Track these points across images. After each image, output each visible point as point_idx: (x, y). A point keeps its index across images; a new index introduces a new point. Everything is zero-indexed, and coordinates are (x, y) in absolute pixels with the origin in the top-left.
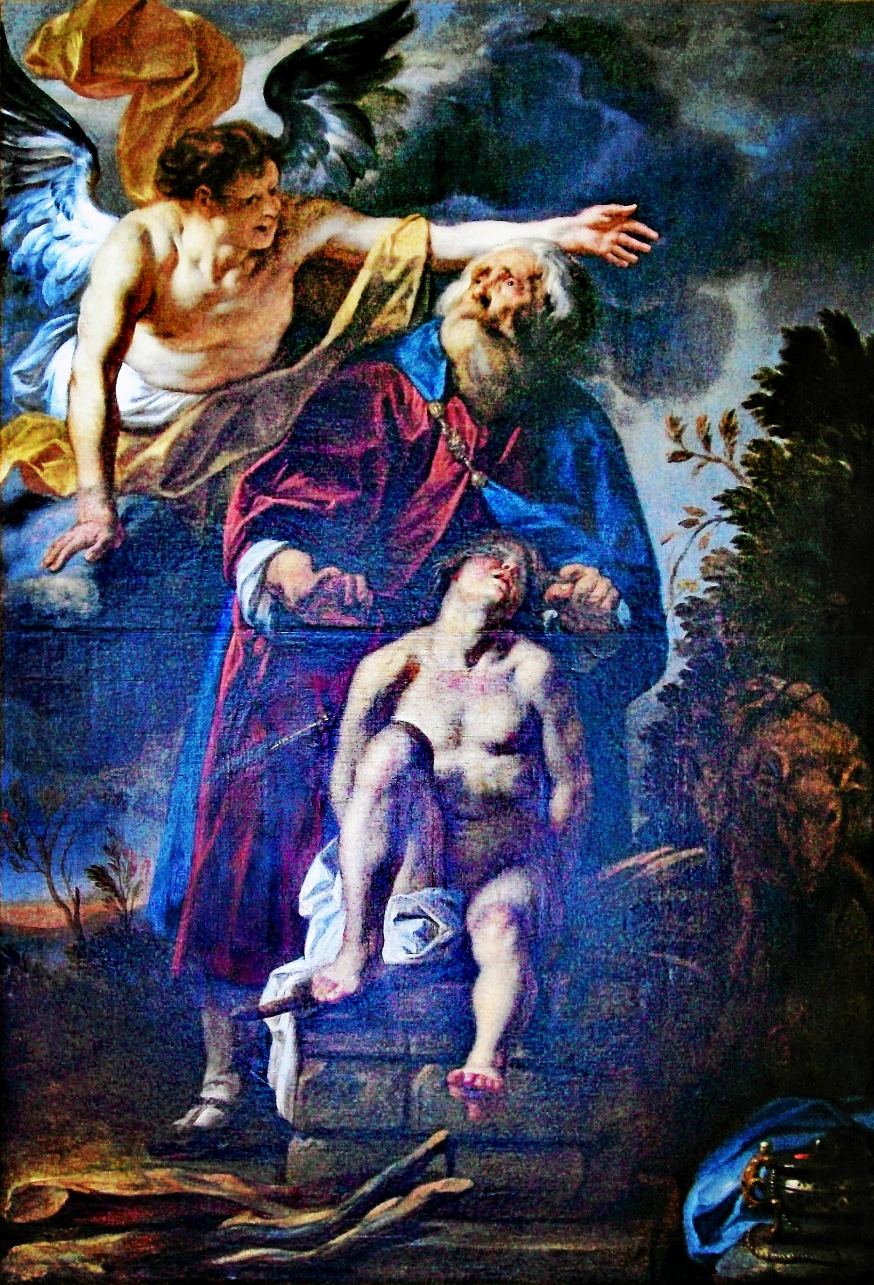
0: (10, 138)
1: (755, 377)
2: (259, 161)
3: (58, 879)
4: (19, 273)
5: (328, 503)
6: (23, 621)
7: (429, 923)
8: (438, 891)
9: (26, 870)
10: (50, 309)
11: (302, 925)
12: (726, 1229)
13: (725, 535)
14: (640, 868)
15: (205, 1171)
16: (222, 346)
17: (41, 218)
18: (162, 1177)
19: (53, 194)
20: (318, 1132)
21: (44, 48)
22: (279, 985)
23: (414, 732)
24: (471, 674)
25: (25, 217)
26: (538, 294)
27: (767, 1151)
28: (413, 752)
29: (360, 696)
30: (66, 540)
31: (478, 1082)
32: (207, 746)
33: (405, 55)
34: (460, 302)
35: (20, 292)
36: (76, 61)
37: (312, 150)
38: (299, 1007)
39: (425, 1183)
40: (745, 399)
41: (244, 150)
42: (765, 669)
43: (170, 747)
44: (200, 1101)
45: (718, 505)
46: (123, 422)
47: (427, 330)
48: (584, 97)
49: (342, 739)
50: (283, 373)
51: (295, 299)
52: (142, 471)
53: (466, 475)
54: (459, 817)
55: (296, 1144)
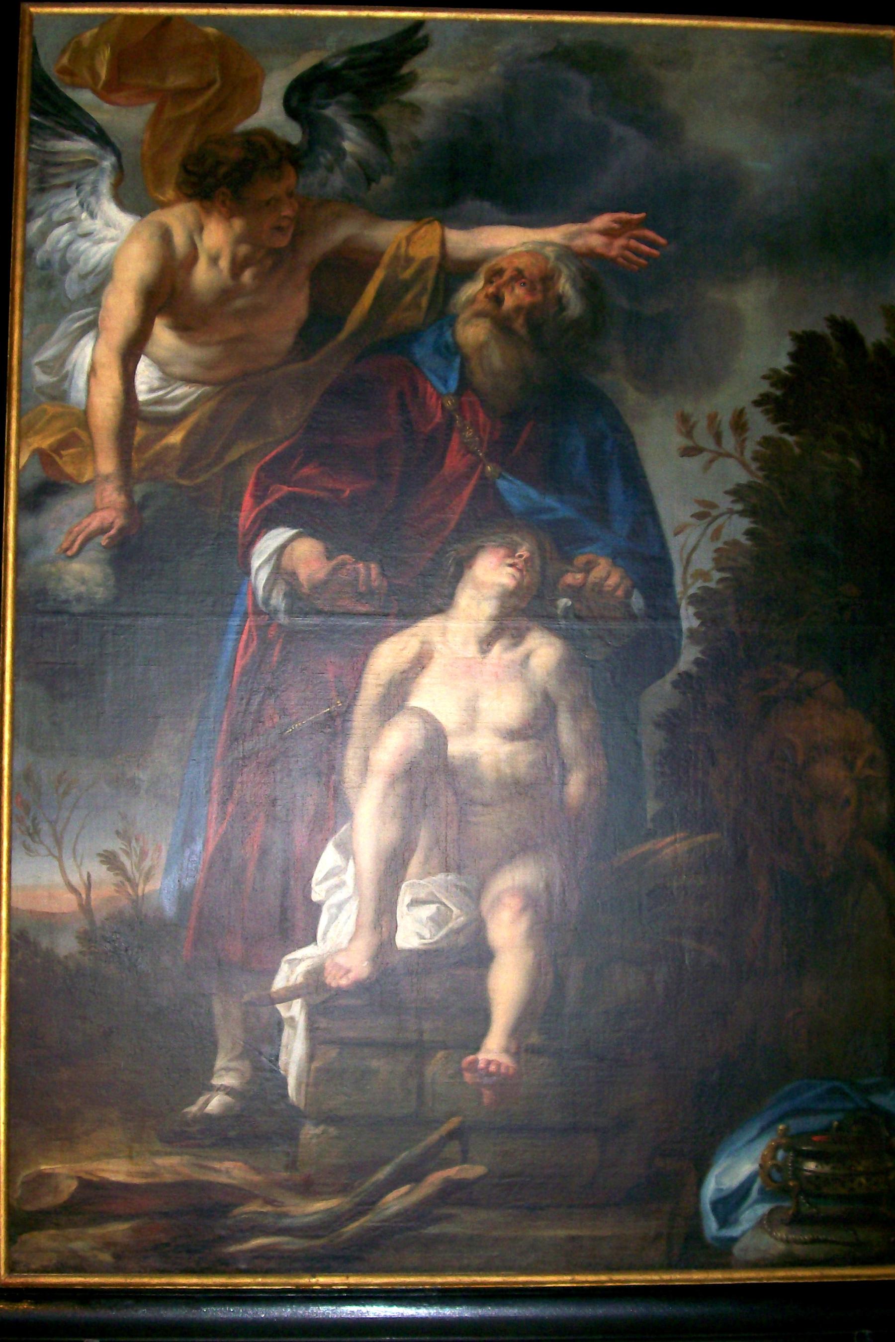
0: (39, 142)
1: (764, 377)
2: (278, 166)
3: (69, 863)
4: (43, 268)
5: (343, 491)
6: (39, 606)
7: (443, 908)
8: (451, 877)
9: (39, 855)
10: (72, 303)
11: (315, 909)
12: (744, 1211)
13: (737, 528)
14: (655, 852)
15: (215, 1159)
16: (239, 339)
17: (65, 216)
18: (171, 1165)
19: (78, 195)
20: (329, 1119)
21: (74, 59)
22: (291, 970)
23: (427, 718)
24: (486, 661)
25: (50, 216)
26: (550, 295)
27: (785, 1133)
28: (427, 739)
29: (374, 682)
30: (83, 526)
31: (493, 1068)
32: (220, 731)
33: (420, 71)
34: (472, 301)
35: (44, 287)
36: (103, 72)
37: (329, 156)
38: (310, 993)
39: (438, 1170)
40: (755, 397)
41: (264, 154)
42: (778, 657)
43: (183, 731)
44: (211, 1089)
45: (730, 498)
46: (141, 411)
47: (441, 327)
48: (594, 113)
49: (355, 724)
50: (300, 365)
51: (311, 296)
52: (159, 459)
53: (480, 466)
54: (472, 802)
55: (309, 1131)
